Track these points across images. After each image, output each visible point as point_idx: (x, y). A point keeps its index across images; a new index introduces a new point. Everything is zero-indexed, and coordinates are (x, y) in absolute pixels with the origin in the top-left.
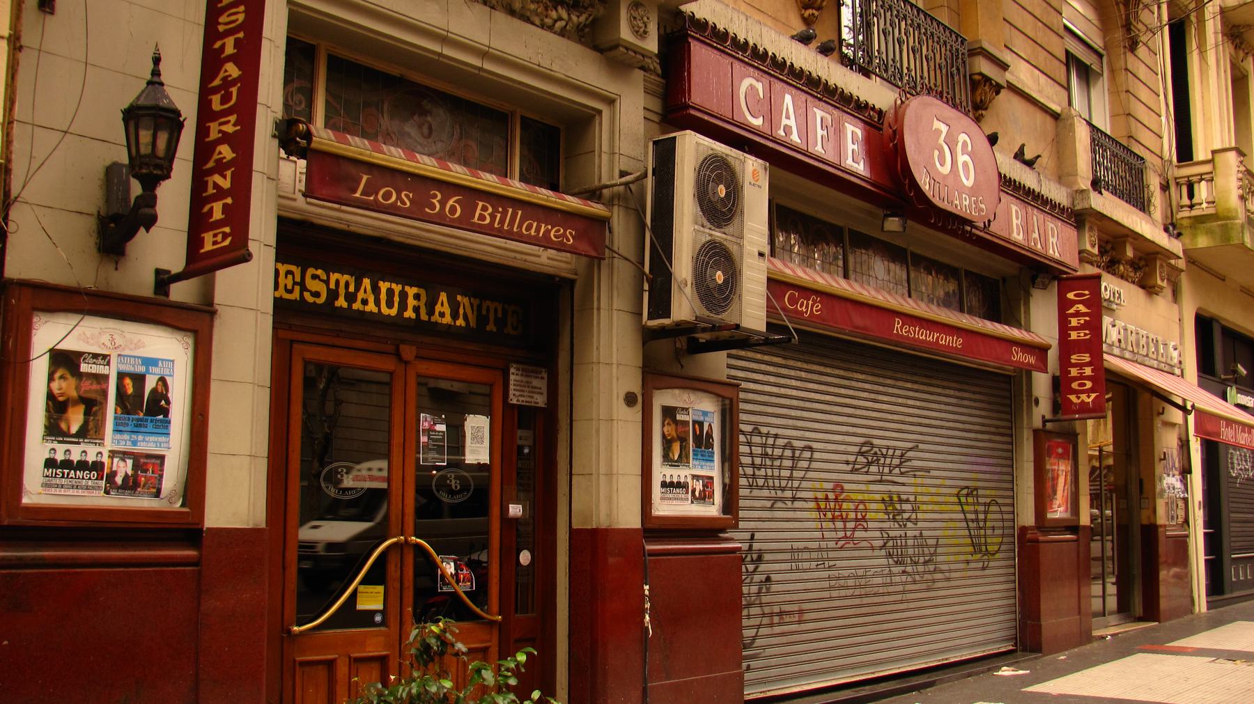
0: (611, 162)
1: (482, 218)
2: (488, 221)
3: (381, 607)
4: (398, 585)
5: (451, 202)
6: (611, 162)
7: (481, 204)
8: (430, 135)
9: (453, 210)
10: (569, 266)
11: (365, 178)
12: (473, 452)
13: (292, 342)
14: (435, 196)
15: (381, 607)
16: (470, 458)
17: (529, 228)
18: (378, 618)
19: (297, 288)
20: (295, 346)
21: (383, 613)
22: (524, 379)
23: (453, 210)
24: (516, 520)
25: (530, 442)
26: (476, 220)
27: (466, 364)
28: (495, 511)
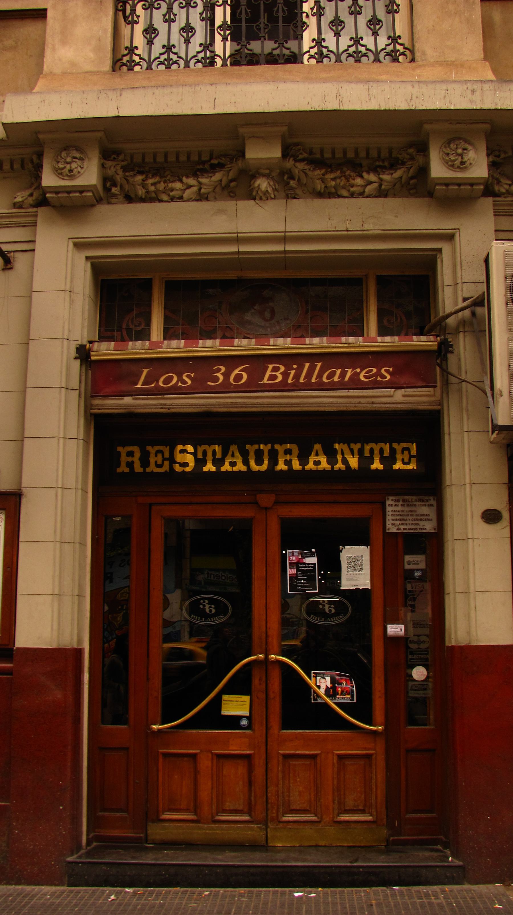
0: (455, 293)
1: (273, 377)
2: (280, 378)
3: (247, 714)
4: (263, 696)
5: (236, 372)
6: (455, 293)
7: (271, 366)
8: (272, 318)
9: (239, 377)
10: (433, 399)
11: (145, 371)
12: (349, 579)
13: (151, 505)
14: (219, 370)
15: (247, 714)
16: (347, 583)
17: (331, 375)
18: (244, 723)
19: (167, 463)
20: (154, 508)
21: (249, 718)
22: (406, 509)
23: (239, 377)
24: (396, 639)
25: (422, 566)
26: (265, 381)
27: (335, 502)
28: (377, 632)
